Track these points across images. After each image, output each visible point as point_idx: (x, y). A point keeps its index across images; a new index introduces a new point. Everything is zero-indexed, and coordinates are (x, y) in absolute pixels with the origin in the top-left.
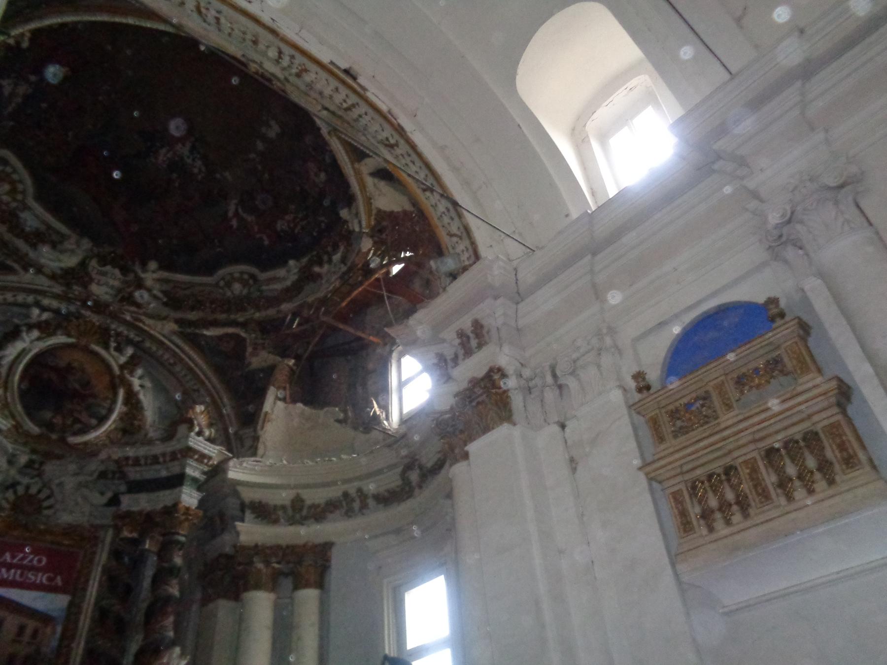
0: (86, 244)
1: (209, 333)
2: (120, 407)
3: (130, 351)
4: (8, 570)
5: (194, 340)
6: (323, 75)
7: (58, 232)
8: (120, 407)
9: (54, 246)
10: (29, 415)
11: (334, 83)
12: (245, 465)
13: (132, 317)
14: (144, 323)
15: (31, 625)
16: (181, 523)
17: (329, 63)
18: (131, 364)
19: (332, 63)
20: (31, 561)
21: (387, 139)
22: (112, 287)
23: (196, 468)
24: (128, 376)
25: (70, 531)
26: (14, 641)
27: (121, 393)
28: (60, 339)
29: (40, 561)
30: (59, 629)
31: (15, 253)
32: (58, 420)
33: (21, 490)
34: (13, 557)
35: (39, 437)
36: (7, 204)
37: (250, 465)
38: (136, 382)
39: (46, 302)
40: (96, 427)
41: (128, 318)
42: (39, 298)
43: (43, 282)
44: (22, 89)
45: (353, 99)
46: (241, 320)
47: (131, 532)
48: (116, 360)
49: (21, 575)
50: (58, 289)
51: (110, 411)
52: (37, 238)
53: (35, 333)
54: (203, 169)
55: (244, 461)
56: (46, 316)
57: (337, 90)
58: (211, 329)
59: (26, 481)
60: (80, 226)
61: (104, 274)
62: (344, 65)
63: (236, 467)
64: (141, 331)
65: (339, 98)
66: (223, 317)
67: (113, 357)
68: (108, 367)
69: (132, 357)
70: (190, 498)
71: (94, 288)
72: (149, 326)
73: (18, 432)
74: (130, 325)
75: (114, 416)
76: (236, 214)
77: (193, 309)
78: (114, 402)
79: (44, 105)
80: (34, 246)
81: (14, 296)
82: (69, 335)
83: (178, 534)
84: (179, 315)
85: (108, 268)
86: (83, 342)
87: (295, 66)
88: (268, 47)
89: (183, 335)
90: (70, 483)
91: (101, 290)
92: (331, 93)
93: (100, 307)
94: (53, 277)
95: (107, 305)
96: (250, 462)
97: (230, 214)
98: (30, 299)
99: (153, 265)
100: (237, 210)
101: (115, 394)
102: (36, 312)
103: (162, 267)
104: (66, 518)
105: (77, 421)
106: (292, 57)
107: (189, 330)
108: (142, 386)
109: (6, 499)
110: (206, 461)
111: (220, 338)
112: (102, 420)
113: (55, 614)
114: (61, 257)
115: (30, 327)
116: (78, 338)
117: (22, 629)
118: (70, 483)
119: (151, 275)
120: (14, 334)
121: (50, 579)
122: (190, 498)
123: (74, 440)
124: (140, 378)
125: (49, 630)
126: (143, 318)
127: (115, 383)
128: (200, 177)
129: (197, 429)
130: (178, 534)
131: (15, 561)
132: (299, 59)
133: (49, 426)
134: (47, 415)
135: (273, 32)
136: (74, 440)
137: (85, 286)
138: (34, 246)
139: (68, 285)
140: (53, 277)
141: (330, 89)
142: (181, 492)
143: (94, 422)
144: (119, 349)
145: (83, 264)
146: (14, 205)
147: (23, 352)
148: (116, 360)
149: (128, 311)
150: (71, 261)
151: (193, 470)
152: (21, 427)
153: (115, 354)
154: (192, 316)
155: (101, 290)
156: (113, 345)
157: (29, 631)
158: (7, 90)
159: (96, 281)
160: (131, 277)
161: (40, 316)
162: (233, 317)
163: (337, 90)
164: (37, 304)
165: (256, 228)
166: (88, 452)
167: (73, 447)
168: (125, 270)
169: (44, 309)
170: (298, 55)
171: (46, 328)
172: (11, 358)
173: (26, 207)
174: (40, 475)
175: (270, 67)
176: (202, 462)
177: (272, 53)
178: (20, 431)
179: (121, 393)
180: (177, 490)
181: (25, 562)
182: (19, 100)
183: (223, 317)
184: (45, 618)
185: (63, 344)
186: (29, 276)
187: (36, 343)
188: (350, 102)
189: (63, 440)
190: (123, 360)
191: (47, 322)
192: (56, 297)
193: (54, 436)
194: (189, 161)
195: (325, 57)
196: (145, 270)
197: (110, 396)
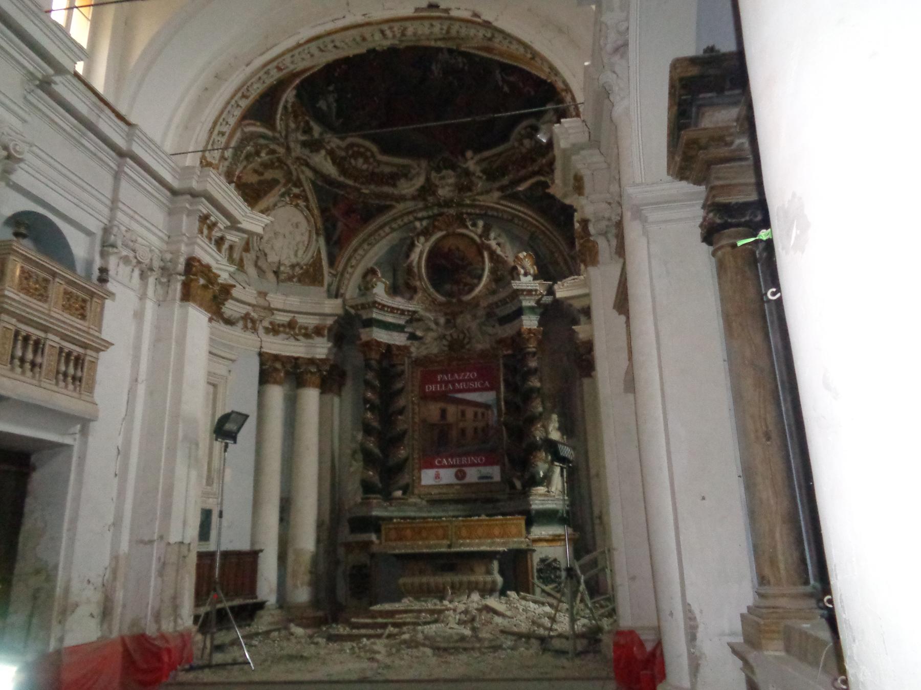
0: (424, 164)
1: (521, 188)
2: (488, 265)
3: (481, 223)
4: (459, 384)
5: (514, 197)
6: (417, 24)
7: (404, 166)
8: (488, 265)
9: (406, 176)
10: (438, 291)
11: (427, 23)
12: (565, 285)
13: (470, 200)
14: (479, 201)
15: (480, 410)
16: (528, 340)
17: (415, 12)
18: (486, 233)
19: (417, 10)
20: (469, 376)
21: (484, 36)
22: (451, 185)
23: (530, 300)
24: (486, 241)
25: (483, 354)
26: (474, 421)
27: (486, 254)
28: (439, 234)
29: (473, 375)
30: (495, 411)
31: (387, 196)
32: (455, 288)
33: (449, 338)
34: (459, 376)
35: (448, 304)
36: (367, 170)
37: (570, 283)
38: (493, 244)
39: (420, 215)
40: (477, 285)
41: (468, 202)
42: (415, 215)
43: (410, 205)
44: (331, 99)
45: (447, 23)
46: (536, 169)
47: (507, 350)
48: (474, 232)
49: (466, 385)
50: (421, 205)
51: (483, 270)
52: (392, 179)
53: (422, 239)
54: (465, 60)
55: (564, 282)
56: (425, 223)
57: (432, 25)
58: (521, 185)
59: (448, 333)
60: (413, 152)
61: (443, 178)
62: (424, 4)
63: (560, 288)
64: (480, 207)
65: (436, 30)
66: (523, 172)
67: (472, 231)
68: (472, 240)
69: (484, 226)
70: (530, 322)
71: (441, 192)
72: (484, 201)
73: (435, 304)
74: (472, 206)
75: (486, 273)
76: (504, 80)
77: (503, 175)
78: (483, 262)
79: (349, 96)
80: (394, 185)
81: (402, 220)
82: (441, 230)
83: (529, 348)
84: (497, 184)
85: (444, 172)
86: (451, 230)
87: (396, 33)
88: (372, 35)
89: (504, 198)
90: (474, 326)
91: (444, 192)
92: (429, 31)
93: (448, 203)
94: (414, 198)
95: (452, 201)
96: (569, 282)
97: (500, 83)
98: (411, 218)
99: (469, 154)
100: (502, 77)
101: (483, 257)
102: (418, 224)
103: (477, 151)
104: (479, 347)
105: (466, 284)
106: (391, 28)
107: (508, 192)
108: (499, 244)
109: (444, 345)
110: (534, 293)
111: (531, 188)
112: (480, 278)
113: (490, 403)
114: (413, 182)
115: (418, 235)
116: (447, 230)
117: (476, 414)
118: (474, 326)
119: (472, 163)
120: (412, 246)
121: (482, 384)
122: (530, 322)
123: (468, 297)
124: (495, 239)
125: (490, 412)
126: (477, 197)
127: (480, 248)
128: (466, 68)
129: (522, 271)
130: (529, 348)
131: (461, 378)
132: (397, 27)
133: (449, 294)
134: (448, 287)
135: (368, 24)
136: (468, 297)
137: (434, 193)
138: (394, 185)
139: (425, 199)
140: (414, 198)
141: (426, 29)
142: (522, 321)
143: (475, 281)
144: (474, 225)
145: (428, 179)
146: (371, 167)
147: (421, 253)
148: (474, 232)
149: (466, 197)
150: (420, 181)
151: (528, 302)
152: (436, 300)
153: (473, 229)
154: (505, 181)
155: (444, 192)
156: (469, 224)
157: (480, 415)
158: (324, 107)
159: (440, 186)
160: (459, 170)
161: (421, 225)
162: (530, 169)
163: (432, 25)
164: (417, 219)
165: (521, 85)
166: (475, 304)
167: (468, 303)
168: (453, 167)
169: (421, 219)
170: (392, 24)
171: (426, 233)
172: (417, 259)
173: (379, 163)
174: (455, 326)
175: (386, 43)
176: (532, 295)
177: (378, 36)
178: (436, 303)
179: (486, 254)
180: (516, 322)
181: (466, 378)
182: (335, 105)
183: (523, 172)
184: (487, 406)
185: (440, 237)
186: (401, 207)
187: (426, 244)
188: (445, 27)
189: (460, 301)
190: (479, 231)
191: (426, 228)
192: (421, 210)
193: (454, 300)
194: (453, 61)
195: (409, 11)
196: (466, 160)
197: (480, 259)
